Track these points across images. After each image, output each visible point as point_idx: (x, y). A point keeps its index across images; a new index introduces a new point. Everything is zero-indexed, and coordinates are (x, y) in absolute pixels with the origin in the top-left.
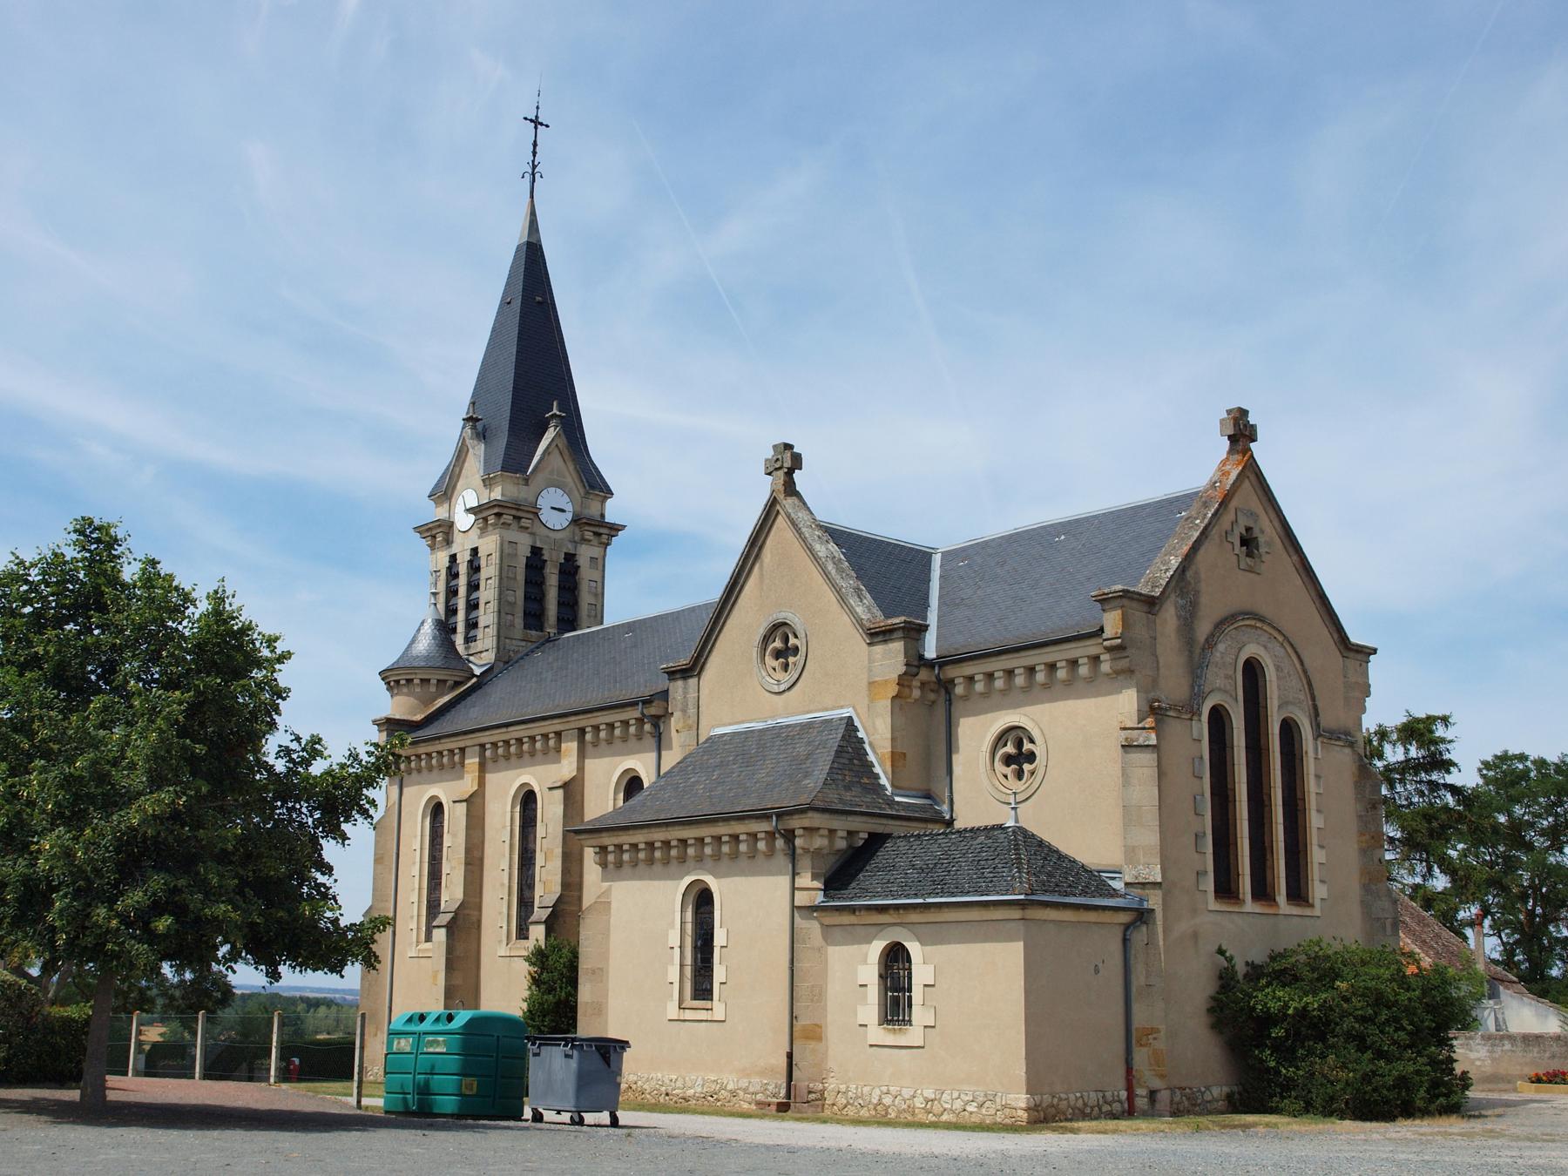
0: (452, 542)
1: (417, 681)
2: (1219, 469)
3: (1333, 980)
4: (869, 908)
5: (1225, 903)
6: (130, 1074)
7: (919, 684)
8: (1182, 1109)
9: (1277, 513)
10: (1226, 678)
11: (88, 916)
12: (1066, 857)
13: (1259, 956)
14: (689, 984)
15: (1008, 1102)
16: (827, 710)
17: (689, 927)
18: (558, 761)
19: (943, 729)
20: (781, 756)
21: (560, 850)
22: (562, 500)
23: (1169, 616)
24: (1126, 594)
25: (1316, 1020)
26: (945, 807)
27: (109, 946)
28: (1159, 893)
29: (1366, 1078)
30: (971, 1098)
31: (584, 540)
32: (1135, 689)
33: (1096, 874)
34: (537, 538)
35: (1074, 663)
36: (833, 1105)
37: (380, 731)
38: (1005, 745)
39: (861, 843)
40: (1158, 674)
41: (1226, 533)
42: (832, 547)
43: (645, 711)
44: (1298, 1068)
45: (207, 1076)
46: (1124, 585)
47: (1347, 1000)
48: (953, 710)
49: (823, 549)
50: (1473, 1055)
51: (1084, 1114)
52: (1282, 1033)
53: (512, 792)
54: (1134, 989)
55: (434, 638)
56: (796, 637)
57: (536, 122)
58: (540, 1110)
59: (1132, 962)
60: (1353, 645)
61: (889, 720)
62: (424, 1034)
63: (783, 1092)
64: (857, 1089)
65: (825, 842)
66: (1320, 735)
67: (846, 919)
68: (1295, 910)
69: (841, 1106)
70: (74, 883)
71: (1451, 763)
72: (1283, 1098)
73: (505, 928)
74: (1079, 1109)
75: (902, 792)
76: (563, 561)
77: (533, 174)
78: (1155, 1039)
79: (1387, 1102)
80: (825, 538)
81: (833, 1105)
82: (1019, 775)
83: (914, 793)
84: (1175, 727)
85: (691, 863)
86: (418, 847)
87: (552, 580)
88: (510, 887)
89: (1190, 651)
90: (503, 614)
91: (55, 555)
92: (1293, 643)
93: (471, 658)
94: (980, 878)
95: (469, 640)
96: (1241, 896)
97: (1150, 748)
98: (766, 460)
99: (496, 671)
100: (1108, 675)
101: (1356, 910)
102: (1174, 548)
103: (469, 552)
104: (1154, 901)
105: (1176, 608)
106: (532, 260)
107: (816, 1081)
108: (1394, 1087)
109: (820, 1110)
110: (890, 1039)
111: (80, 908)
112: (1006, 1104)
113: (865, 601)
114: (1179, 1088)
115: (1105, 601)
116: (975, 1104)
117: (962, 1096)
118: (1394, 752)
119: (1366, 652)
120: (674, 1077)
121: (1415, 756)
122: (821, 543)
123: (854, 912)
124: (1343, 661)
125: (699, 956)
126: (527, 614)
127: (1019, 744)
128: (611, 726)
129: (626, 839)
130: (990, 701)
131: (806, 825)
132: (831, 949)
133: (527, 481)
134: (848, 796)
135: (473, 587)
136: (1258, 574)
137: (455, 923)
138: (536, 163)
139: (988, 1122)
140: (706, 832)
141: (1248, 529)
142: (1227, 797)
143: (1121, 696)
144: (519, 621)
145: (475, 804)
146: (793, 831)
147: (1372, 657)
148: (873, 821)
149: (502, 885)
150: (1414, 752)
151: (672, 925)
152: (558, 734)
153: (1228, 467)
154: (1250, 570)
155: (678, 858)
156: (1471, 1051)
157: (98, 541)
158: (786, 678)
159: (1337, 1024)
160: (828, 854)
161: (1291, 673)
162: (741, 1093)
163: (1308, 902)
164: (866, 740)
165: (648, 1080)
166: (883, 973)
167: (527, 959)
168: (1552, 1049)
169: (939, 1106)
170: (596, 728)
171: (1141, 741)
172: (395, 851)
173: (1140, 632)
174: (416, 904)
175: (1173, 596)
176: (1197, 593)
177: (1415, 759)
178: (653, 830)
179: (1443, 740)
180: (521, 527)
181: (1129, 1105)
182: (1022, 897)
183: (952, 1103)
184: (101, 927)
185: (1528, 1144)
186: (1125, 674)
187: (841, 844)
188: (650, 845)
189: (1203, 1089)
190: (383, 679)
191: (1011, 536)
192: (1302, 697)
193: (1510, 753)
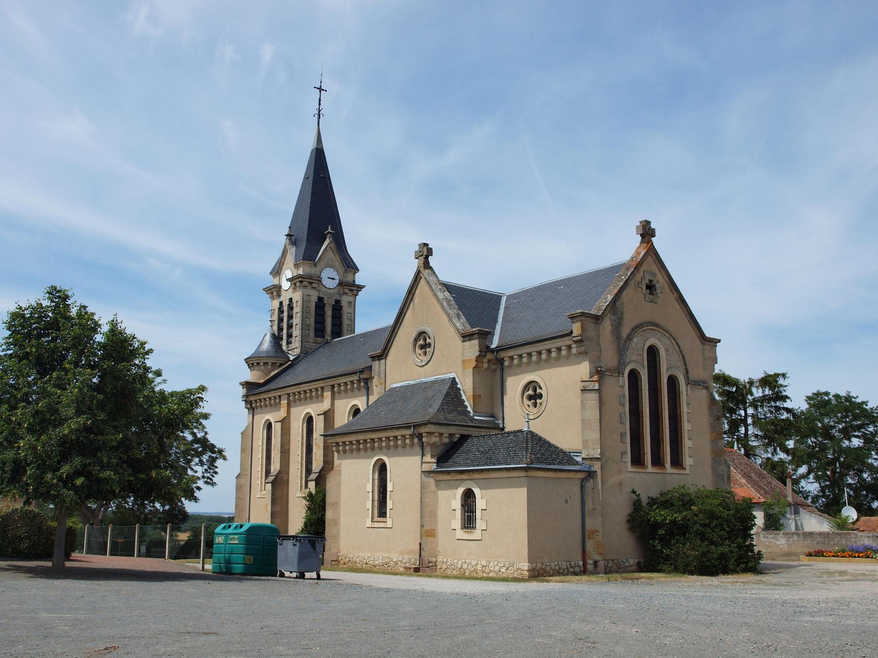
0: (281, 295)
1: (262, 364)
2: (636, 251)
3: (690, 506)
4: (456, 472)
5: (675, 468)
6: (108, 555)
7: (487, 361)
8: (613, 570)
9: (666, 272)
10: (637, 355)
11: (43, 478)
12: (553, 445)
13: (654, 494)
14: (377, 510)
15: (520, 567)
16: (443, 374)
17: (376, 482)
18: (322, 401)
19: (499, 383)
20: (420, 397)
21: (322, 445)
22: (333, 274)
23: (607, 325)
24: (583, 314)
25: (680, 526)
26: (500, 422)
27: (52, 492)
28: (599, 463)
29: (704, 555)
30: (503, 565)
31: (345, 293)
32: (588, 362)
33: (568, 454)
34: (321, 292)
35: (559, 349)
36: (441, 568)
37: (243, 388)
38: (528, 390)
39: (456, 440)
40: (601, 354)
41: (638, 283)
42: (447, 294)
43: (361, 376)
44: (672, 550)
45: (112, 554)
46: (582, 310)
47: (697, 515)
48: (504, 373)
49: (442, 295)
50: (778, 543)
51: (558, 573)
52: (663, 532)
53: (302, 417)
54: (586, 511)
55: (271, 342)
56: (430, 338)
57: (320, 89)
58: (283, 571)
59: (586, 497)
60: (707, 338)
61: (472, 378)
62: (229, 534)
63: (418, 563)
64: (451, 560)
65: (437, 439)
66: (689, 383)
67: (446, 477)
68: (675, 471)
69: (444, 569)
70: (37, 462)
71: (787, 397)
72: (664, 564)
73: (299, 483)
74: (556, 571)
75: (479, 414)
76: (334, 304)
77: (319, 114)
78: (597, 535)
79: (715, 566)
80: (443, 289)
81: (441, 568)
82: (535, 405)
83: (485, 415)
84: (610, 381)
85: (377, 450)
86: (261, 444)
87: (329, 313)
88: (302, 463)
89: (618, 342)
90: (304, 330)
91: (37, 304)
92: (674, 337)
93: (290, 352)
94: (508, 456)
95: (288, 343)
96: (646, 464)
97: (595, 391)
98: (416, 252)
99: (300, 358)
100: (576, 355)
101: (709, 471)
102: (610, 291)
103: (288, 300)
104: (597, 467)
105: (611, 321)
106: (319, 159)
107: (432, 557)
108: (718, 558)
109: (434, 571)
110: (466, 536)
111: (39, 474)
112: (519, 568)
113: (461, 320)
114: (612, 560)
115: (573, 318)
116: (504, 568)
117: (499, 564)
118: (758, 392)
119: (715, 342)
120: (370, 555)
121: (768, 394)
122: (441, 292)
123: (449, 474)
124: (703, 346)
125: (381, 496)
126: (316, 330)
127: (535, 390)
128: (346, 384)
129: (347, 439)
130: (522, 368)
131: (428, 431)
132: (440, 492)
133: (315, 265)
134: (449, 416)
135: (290, 317)
136: (656, 303)
137: (276, 481)
138: (320, 109)
139: (510, 577)
140: (382, 435)
141: (650, 281)
142: (639, 415)
143: (581, 365)
144: (312, 334)
145: (285, 423)
146: (422, 434)
147: (718, 344)
148: (463, 429)
149: (298, 462)
150: (767, 392)
151: (368, 481)
152: (322, 388)
153: (640, 250)
154: (652, 301)
155: (371, 448)
156: (778, 540)
157: (59, 297)
158: (425, 359)
159: (691, 527)
160: (439, 446)
161: (674, 352)
162: (399, 563)
163: (682, 467)
164: (461, 389)
165: (358, 556)
166: (463, 503)
167: (305, 498)
168: (818, 539)
169: (488, 569)
170: (339, 385)
171: (590, 388)
172: (250, 446)
173: (591, 333)
174: (260, 472)
175: (609, 315)
176: (622, 313)
177: (768, 395)
178: (359, 434)
179: (781, 386)
180: (313, 287)
181: (584, 569)
182: (525, 465)
183: (495, 567)
184: (49, 483)
185: (773, 587)
186: (583, 354)
187: (446, 440)
188: (358, 442)
189: (624, 560)
190: (246, 363)
191: (539, 286)
192: (680, 364)
193: (821, 392)
